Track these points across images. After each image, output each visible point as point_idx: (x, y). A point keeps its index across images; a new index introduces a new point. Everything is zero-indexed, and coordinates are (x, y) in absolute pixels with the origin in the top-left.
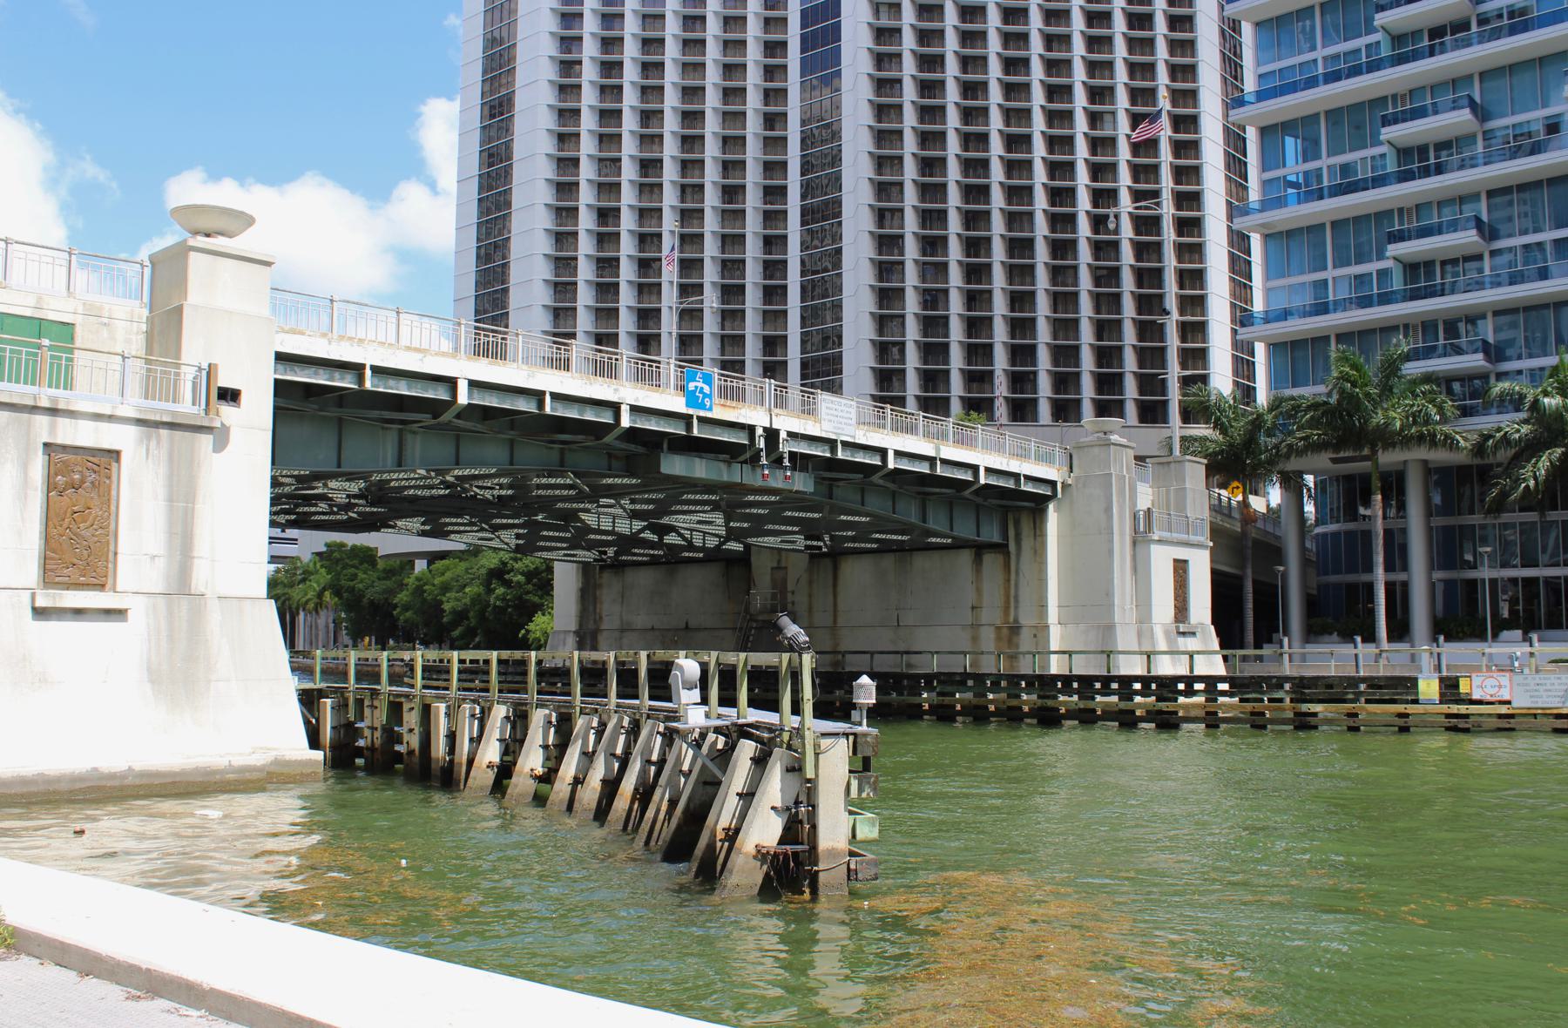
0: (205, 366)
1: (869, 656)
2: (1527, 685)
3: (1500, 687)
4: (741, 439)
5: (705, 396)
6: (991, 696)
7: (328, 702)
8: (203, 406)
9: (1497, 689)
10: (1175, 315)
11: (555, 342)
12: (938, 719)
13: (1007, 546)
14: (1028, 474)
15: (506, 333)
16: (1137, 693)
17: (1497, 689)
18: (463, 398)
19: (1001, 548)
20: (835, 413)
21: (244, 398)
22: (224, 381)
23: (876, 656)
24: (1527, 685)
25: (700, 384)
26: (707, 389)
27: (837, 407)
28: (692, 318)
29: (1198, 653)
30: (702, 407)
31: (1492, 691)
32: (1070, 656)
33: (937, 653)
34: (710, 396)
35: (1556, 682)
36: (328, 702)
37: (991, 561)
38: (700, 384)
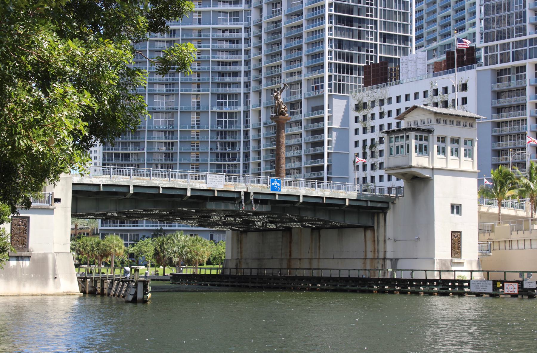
0: (51, 193)
1: (357, 271)
2: (475, 284)
3: (514, 288)
4: (235, 196)
5: (278, 187)
6: (409, 288)
7: (88, 280)
8: (50, 204)
9: (513, 289)
10: (528, 116)
11: (307, 181)
12: (476, 296)
13: (374, 227)
14: (164, 186)
15: (260, 178)
16: (466, 287)
17: (513, 289)
18: (301, 200)
19: (372, 228)
20: (214, 180)
21: (62, 200)
22: (56, 197)
23: (341, 271)
24: (475, 284)
25: (276, 183)
26: (278, 184)
27: (215, 178)
28: (374, 167)
29: (443, 271)
30: (277, 190)
31: (512, 290)
32: (440, 273)
33: (403, 270)
34: (280, 187)
35: (484, 283)
36: (88, 280)
37: (369, 233)
38: (276, 183)
